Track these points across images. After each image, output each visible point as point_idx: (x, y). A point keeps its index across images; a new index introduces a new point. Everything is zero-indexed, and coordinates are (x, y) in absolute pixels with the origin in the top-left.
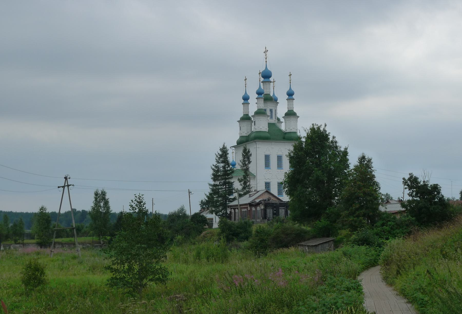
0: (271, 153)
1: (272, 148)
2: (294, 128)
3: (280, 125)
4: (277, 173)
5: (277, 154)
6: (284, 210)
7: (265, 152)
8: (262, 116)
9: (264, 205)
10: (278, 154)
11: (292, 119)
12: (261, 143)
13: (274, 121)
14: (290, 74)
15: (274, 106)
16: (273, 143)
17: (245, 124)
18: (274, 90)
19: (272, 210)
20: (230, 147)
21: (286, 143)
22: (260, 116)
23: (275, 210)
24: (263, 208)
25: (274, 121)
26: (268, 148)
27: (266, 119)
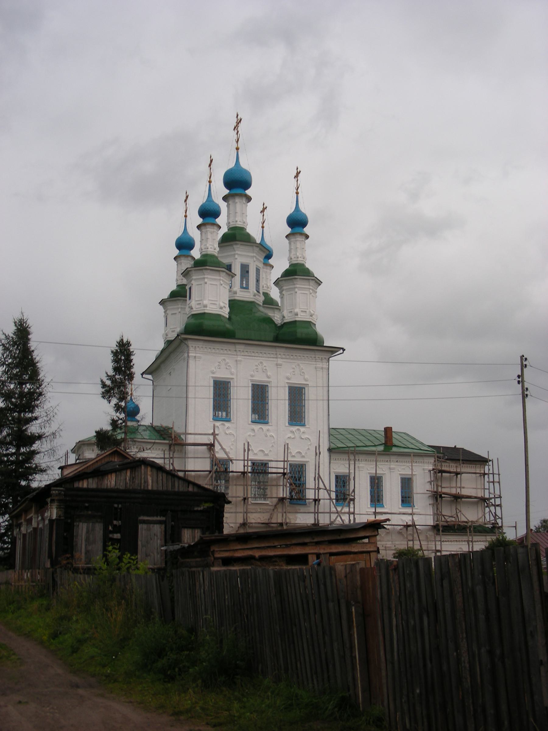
0: (232, 374)
1: (236, 361)
2: (306, 312)
3: (275, 315)
4: (249, 434)
5: (252, 381)
6: (157, 529)
7: (213, 373)
8: (209, 271)
9: (59, 501)
10: (254, 378)
11: (300, 284)
12: (200, 344)
13: (252, 297)
14: (297, 178)
15: (253, 257)
16: (240, 347)
17: (178, 308)
18: (263, 231)
19: (99, 528)
20: (142, 374)
21: (278, 350)
22: (204, 271)
23: (116, 529)
24: (54, 517)
25: (252, 297)
26: (224, 360)
27: (220, 280)
